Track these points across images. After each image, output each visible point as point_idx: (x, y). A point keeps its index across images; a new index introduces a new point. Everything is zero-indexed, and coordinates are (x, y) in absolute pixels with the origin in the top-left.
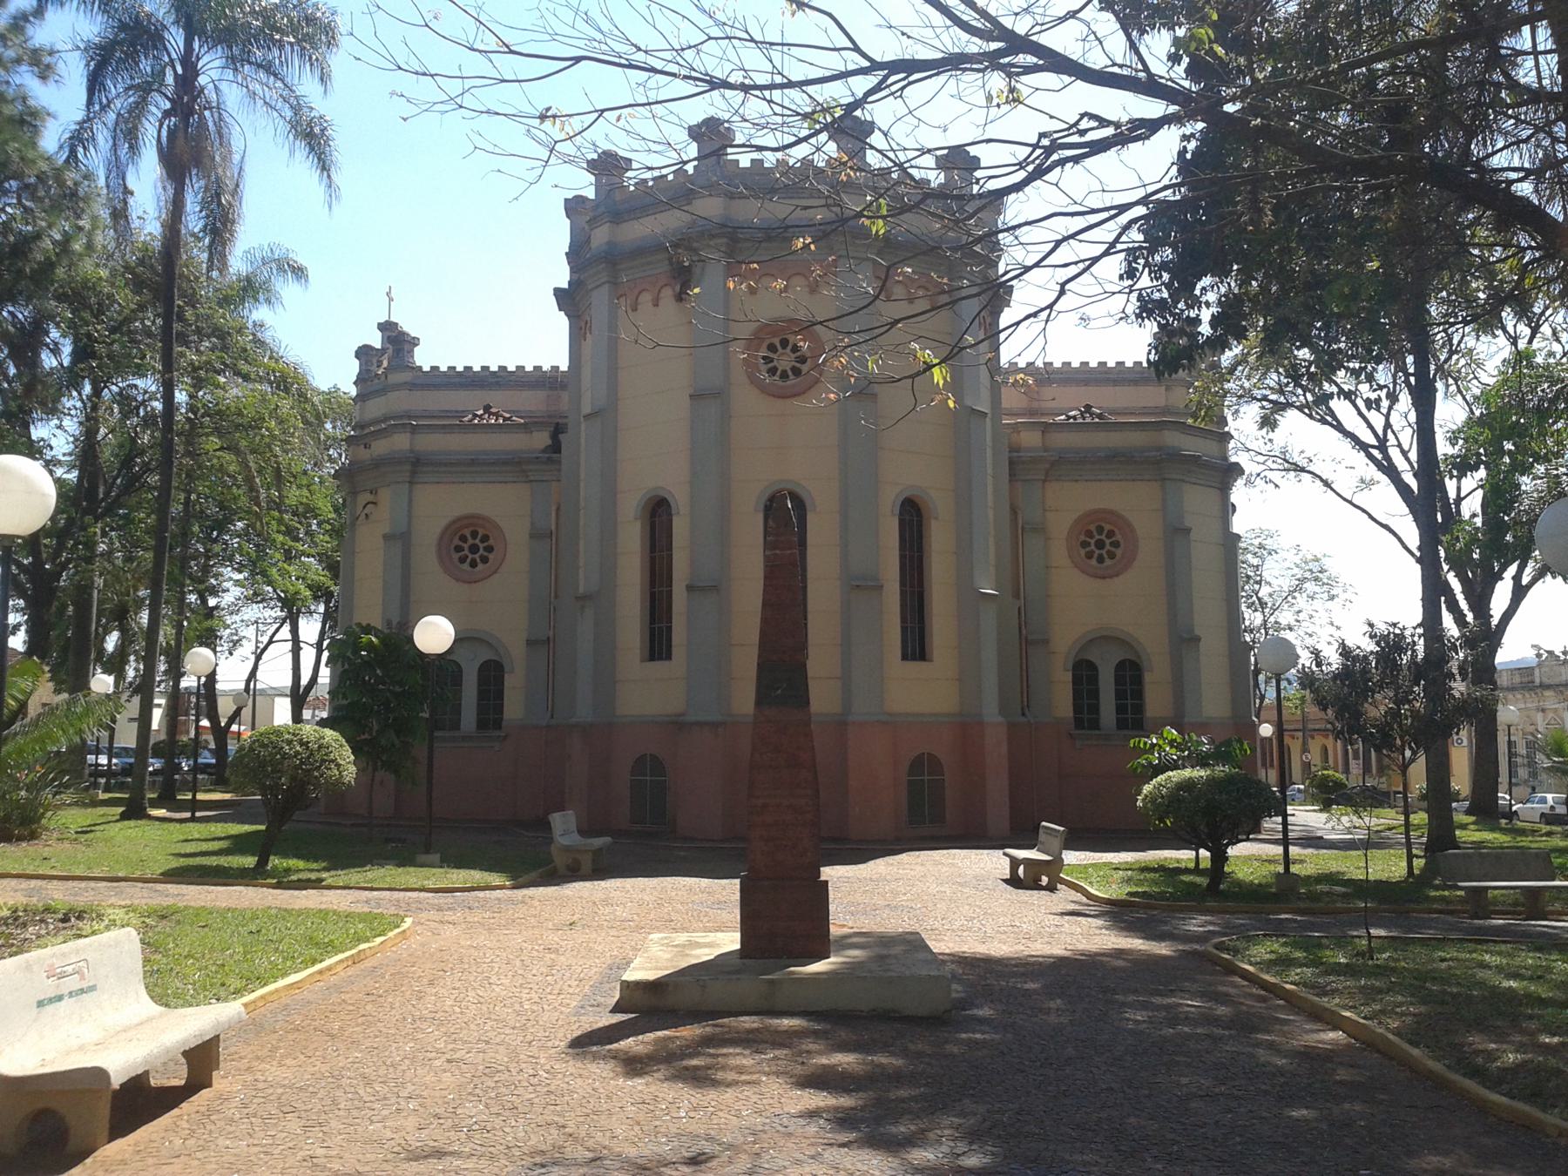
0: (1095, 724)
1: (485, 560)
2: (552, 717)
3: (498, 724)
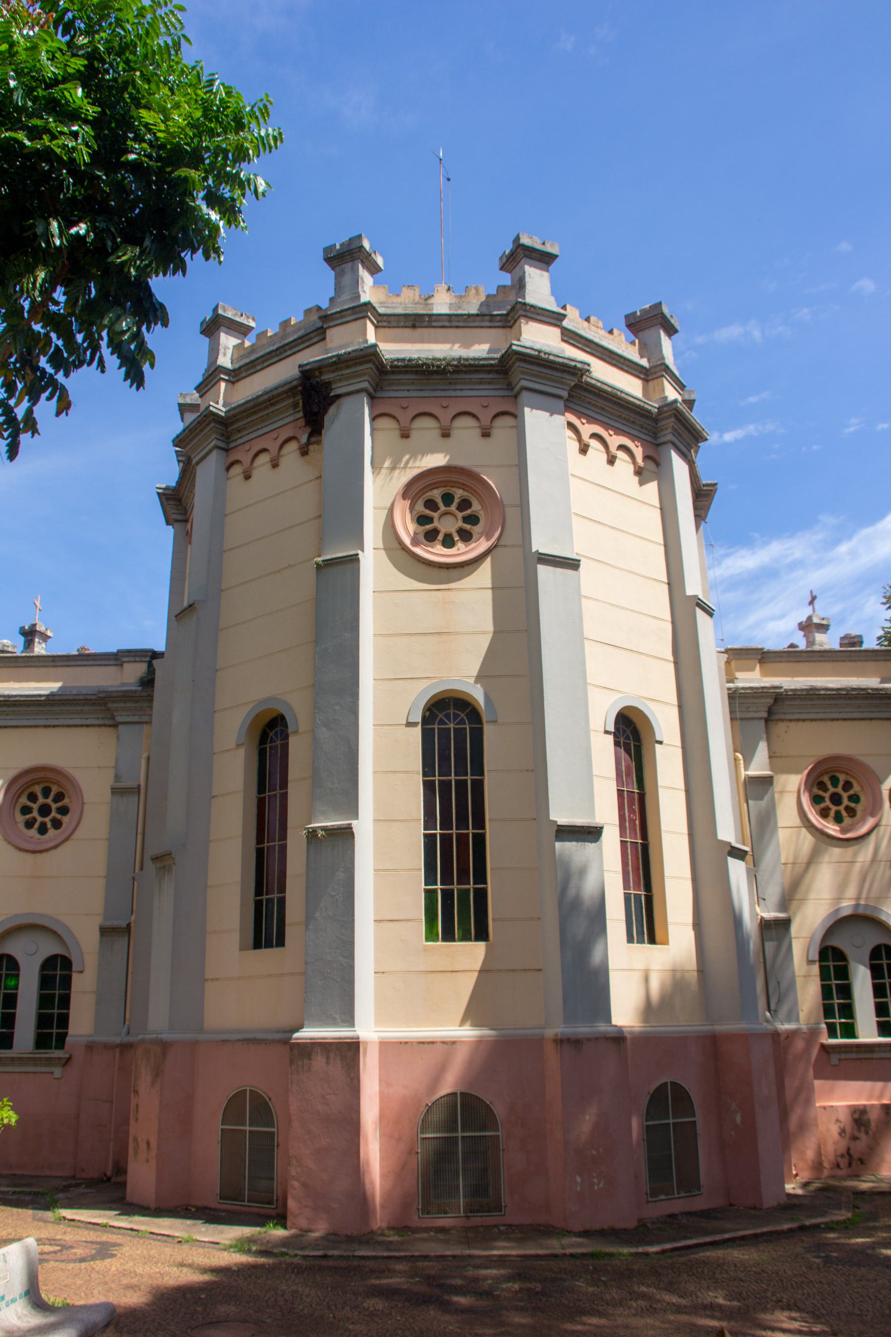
1: (57, 824)
2: (128, 1033)
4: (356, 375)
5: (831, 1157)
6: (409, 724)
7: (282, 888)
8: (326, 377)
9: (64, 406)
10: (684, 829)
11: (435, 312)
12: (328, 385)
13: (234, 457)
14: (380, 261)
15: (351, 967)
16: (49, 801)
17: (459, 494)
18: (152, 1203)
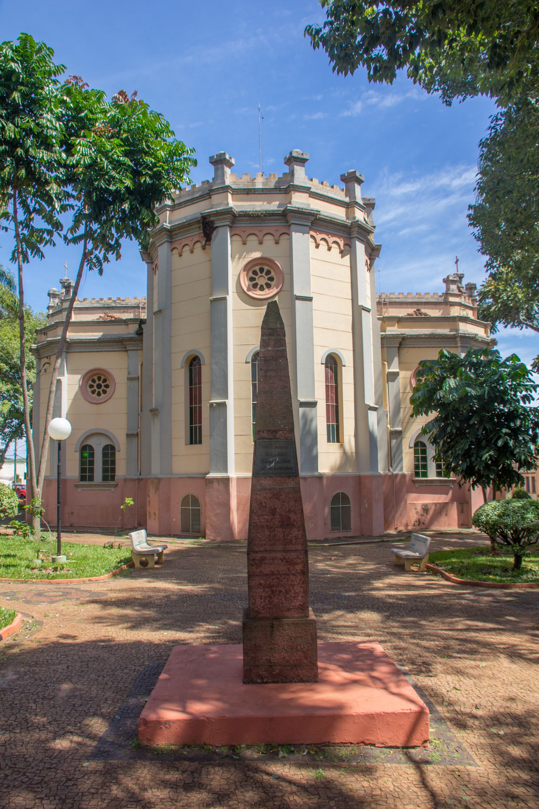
0: (91, 478)
1: (105, 392)
3: (113, 478)
4: (224, 219)
5: (413, 522)
6: (247, 363)
7: (200, 422)
8: (212, 219)
9: (118, 257)
10: (353, 399)
11: (257, 187)
12: (213, 222)
13: (175, 245)
14: (233, 161)
15: (226, 452)
16: (101, 382)
17: (266, 268)
18: (158, 534)
